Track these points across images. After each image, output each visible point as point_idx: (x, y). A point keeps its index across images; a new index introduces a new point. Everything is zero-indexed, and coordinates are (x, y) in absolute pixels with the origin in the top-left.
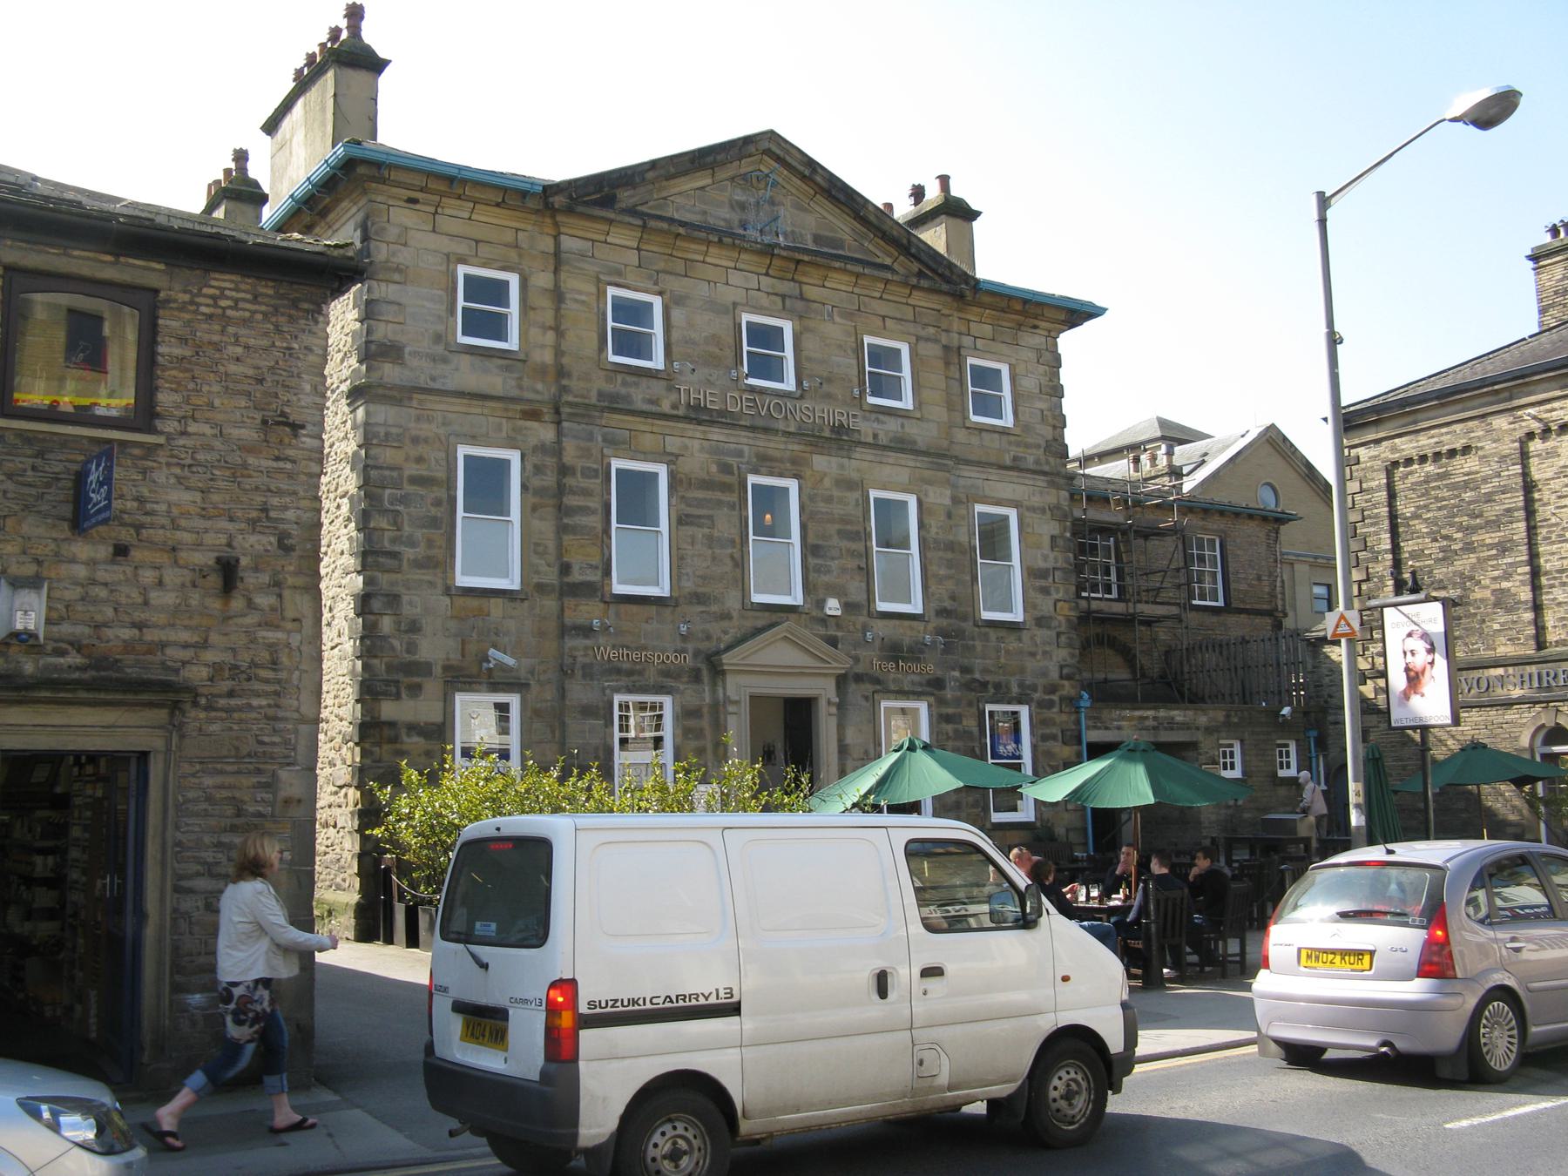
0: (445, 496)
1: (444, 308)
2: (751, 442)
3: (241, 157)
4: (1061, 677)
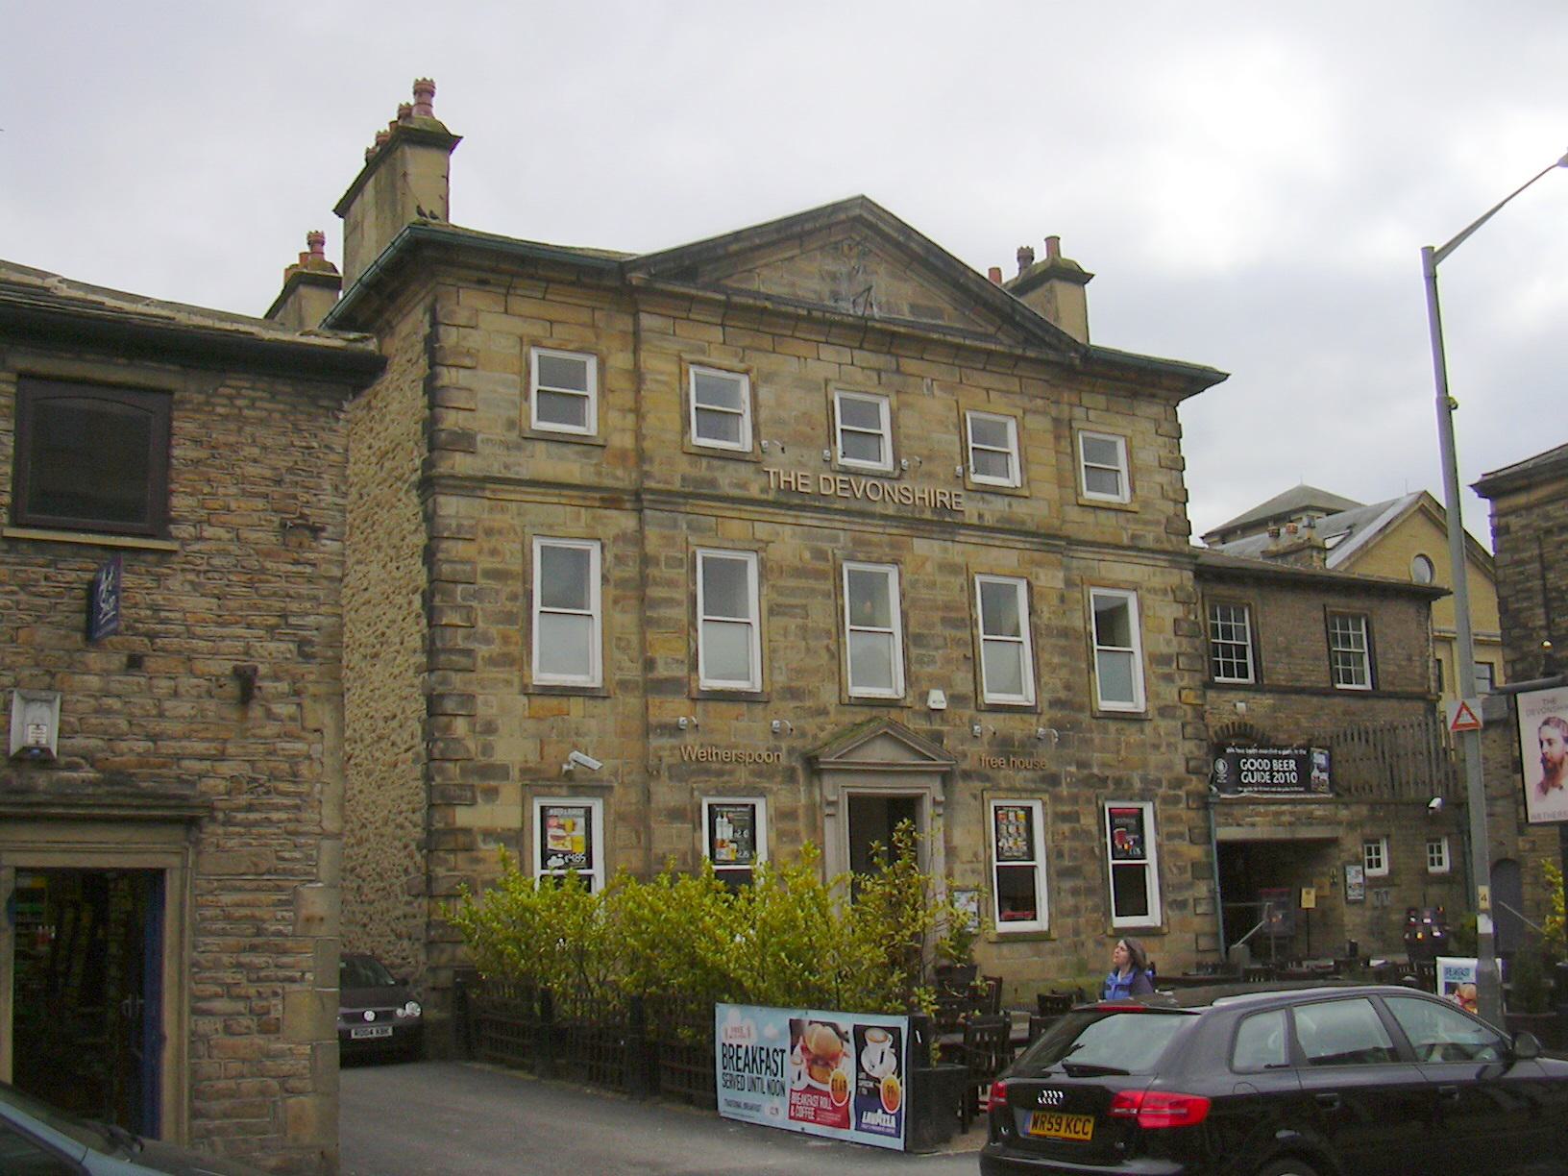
0: (520, 591)
1: (518, 392)
2: (847, 526)
3: (316, 241)
4: (1188, 771)
